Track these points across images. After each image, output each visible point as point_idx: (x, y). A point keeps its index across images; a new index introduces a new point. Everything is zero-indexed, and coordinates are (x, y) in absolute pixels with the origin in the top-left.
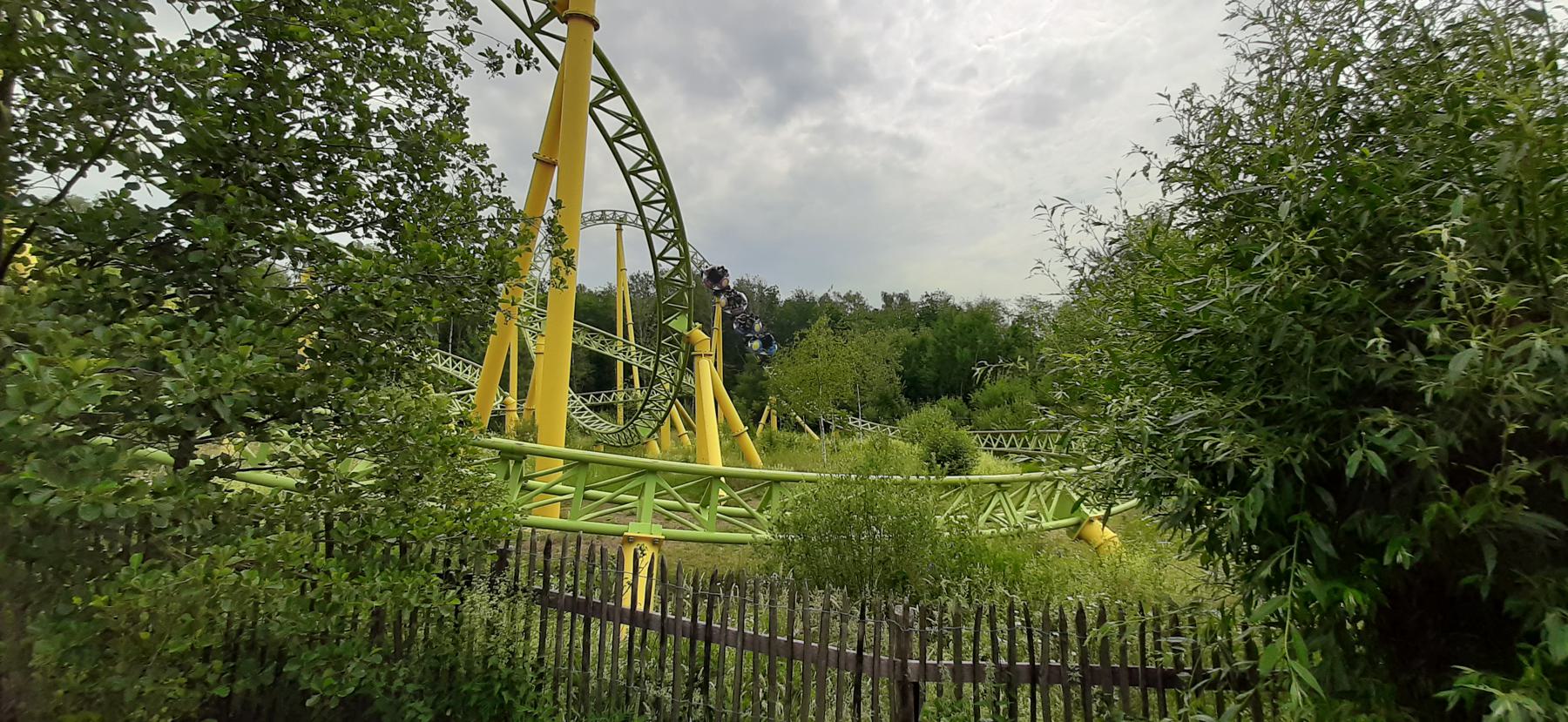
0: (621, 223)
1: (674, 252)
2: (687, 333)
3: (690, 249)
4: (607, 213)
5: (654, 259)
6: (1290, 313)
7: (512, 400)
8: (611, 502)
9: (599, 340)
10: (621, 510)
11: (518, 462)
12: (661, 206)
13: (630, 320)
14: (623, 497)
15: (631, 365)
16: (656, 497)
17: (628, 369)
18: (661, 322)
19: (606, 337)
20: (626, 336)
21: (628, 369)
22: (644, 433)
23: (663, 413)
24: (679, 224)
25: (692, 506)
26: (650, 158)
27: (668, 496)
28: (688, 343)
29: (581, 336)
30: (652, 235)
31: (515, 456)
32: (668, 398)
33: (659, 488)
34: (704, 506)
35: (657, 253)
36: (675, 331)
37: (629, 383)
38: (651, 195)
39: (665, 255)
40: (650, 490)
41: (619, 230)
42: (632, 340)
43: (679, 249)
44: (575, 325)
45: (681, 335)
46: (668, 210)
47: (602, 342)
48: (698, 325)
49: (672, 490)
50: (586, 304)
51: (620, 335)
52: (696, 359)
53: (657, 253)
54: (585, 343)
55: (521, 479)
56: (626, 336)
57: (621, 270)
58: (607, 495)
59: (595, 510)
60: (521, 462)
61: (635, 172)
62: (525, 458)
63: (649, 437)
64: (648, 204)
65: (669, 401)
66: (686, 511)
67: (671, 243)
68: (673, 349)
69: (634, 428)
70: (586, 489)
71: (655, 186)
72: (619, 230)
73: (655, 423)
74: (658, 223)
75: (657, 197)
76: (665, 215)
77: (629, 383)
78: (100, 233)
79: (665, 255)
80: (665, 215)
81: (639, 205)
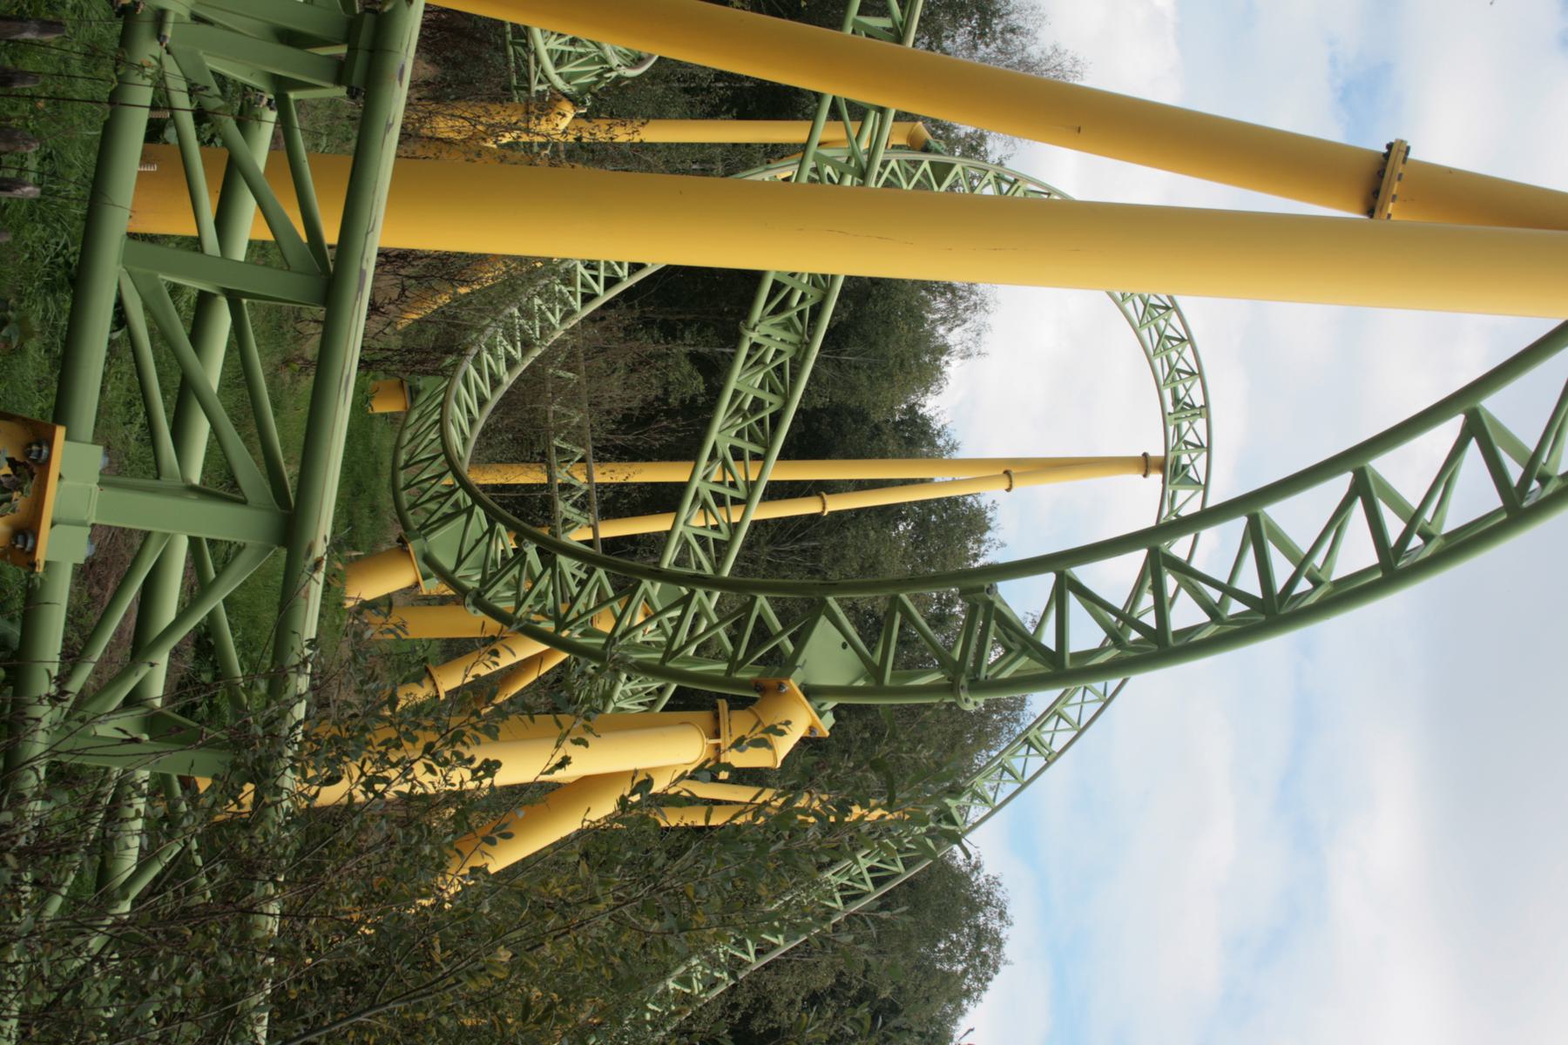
0: (1170, 469)
1: (1085, 634)
2: (793, 684)
3: (1113, 683)
4: (1200, 424)
5: (1058, 563)
6: (244, 697)
7: (563, 123)
8: (184, 393)
9: (766, 396)
10: (150, 427)
11: (339, 69)
12: (1249, 582)
13: (838, 504)
14: (201, 430)
15: (812, 117)
16: (194, 543)
17: (666, 499)
18: (833, 587)
19: (776, 419)
20: (778, 491)
21: (666, 499)
22: (443, 544)
23: (507, 606)
24: (1187, 646)
25: (157, 677)
26: (1416, 541)
27: (197, 587)
28: (759, 687)
29: (779, 334)
30: (1139, 557)
31: (361, 58)
32: (561, 623)
33: (226, 554)
34: (153, 723)
35: (1083, 573)
36: (799, 639)
37: (619, 502)
38: (1287, 549)
39: (1074, 603)
40: (219, 522)
41: (1146, 464)
42: (761, 512)
43: (1101, 650)
44: (821, 282)
45: (781, 663)
46: (1236, 607)
47: (758, 405)
48: (825, 725)
49: (216, 602)
50: (915, 315)
51: (779, 471)
52: (704, 716)
53: (1083, 573)
54: (756, 346)
55: (281, 85)
56: (778, 491)
57: (1009, 471)
58: (212, 371)
59: (160, 335)
60: (338, 82)
61: (1363, 489)
62: (352, 93)
63: (428, 559)
64: (1256, 535)
65: (549, 626)
66: (140, 644)
67: (1117, 621)
68: (735, 640)
69: (458, 510)
70: (234, 299)
71: (1318, 561)
72: (1146, 464)
73: (473, 581)
74: (1182, 569)
75: (1282, 570)
76: (1215, 595)
77: (619, 502)
78: (476, 1032)
79: (1074, 603)
80: (1215, 595)
81: (1249, 504)
